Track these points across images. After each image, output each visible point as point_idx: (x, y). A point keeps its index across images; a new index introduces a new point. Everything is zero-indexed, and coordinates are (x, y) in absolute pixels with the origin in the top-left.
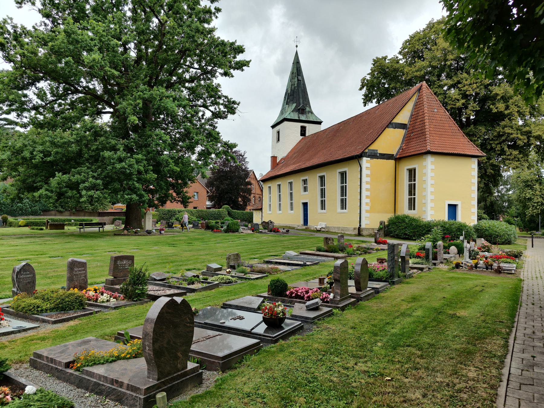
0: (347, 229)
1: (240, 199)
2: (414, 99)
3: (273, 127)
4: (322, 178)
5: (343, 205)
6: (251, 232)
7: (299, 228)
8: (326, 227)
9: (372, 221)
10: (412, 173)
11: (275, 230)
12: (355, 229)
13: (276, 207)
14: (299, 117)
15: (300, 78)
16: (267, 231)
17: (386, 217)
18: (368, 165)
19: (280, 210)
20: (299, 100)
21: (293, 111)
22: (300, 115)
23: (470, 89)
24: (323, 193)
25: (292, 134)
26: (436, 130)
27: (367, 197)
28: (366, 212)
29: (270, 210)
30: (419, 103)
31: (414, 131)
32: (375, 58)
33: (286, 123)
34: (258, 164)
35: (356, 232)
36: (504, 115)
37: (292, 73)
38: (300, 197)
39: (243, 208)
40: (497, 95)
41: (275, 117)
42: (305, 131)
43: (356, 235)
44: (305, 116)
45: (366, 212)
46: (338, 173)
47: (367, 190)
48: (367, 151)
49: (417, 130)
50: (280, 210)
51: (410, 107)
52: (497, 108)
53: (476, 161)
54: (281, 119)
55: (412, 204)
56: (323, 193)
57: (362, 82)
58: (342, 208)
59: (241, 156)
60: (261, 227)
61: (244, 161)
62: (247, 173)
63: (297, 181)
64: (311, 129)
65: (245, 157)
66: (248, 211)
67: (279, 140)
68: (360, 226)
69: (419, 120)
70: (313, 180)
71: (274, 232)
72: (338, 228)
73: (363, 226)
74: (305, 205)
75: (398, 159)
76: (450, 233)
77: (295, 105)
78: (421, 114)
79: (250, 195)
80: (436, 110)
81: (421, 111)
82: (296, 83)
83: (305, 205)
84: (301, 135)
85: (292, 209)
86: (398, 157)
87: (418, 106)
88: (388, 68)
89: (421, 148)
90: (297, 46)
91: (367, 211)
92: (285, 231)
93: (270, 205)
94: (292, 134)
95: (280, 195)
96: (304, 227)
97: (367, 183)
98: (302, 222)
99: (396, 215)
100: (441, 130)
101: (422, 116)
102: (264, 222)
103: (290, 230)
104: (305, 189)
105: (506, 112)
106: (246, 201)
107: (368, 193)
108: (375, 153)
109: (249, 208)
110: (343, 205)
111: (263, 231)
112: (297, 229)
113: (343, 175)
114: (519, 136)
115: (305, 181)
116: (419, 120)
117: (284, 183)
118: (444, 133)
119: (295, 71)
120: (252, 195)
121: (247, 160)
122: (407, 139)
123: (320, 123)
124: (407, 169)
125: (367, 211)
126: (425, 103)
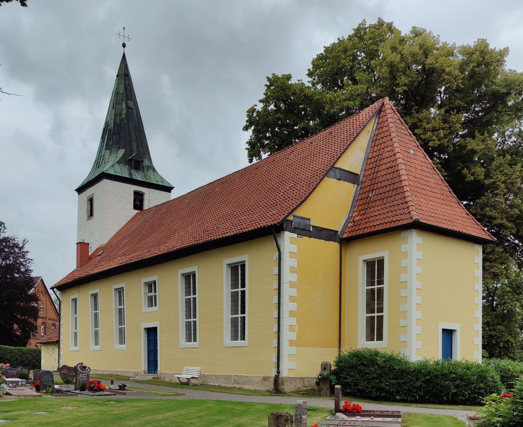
0: (248, 380)
1: (15, 326)
2: (371, 127)
3: (80, 190)
4: (190, 279)
5: (239, 330)
6: (33, 392)
7: (137, 378)
8: (202, 376)
9: (304, 362)
10: (375, 270)
11: (94, 387)
12: (265, 379)
13: (84, 338)
14: (130, 174)
15: (131, 104)
16: (72, 387)
17: (331, 357)
18: (294, 248)
19: (96, 343)
21: (118, 162)
22: (133, 171)
23: (434, 138)
24: (191, 308)
25: (117, 204)
26: (419, 185)
27: (292, 313)
28: (290, 345)
29: (76, 345)
30: (379, 137)
31: (376, 186)
32: (271, 77)
34: (50, 263)
35: (270, 386)
36: (483, 185)
37: (116, 93)
38: (141, 316)
39: (23, 341)
40: (473, 152)
41: (84, 174)
42: (142, 201)
43: (271, 393)
44: (141, 173)
45: (290, 345)
46: (180, 276)
47: (292, 299)
48: (291, 218)
49: (383, 184)
50: (96, 343)
51: (363, 142)
52: (473, 174)
53: (479, 249)
54: (97, 173)
55: (375, 329)
56: (191, 308)
57: (248, 116)
58: (189, 339)
59: (17, 247)
60: (57, 378)
61: (23, 257)
62: (30, 282)
63: (134, 286)
64: (153, 198)
65: (25, 250)
66: (33, 347)
67: (91, 214)
68: (278, 372)
69: (384, 167)
70: (169, 281)
71: (91, 389)
72: (227, 378)
73: (285, 373)
74: (152, 333)
75: (347, 241)
76: (466, 386)
77: (121, 152)
78: (387, 155)
79: (36, 321)
80: (412, 152)
81: (389, 149)
82: (124, 112)
83: (152, 333)
84: (136, 207)
85: (122, 341)
86: (345, 236)
87: (379, 141)
88: (294, 94)
89: (398, 218)
90: (124, 45)
91: (291, 343)
92: (115, 386)
93: (76, 334)
94: (117, 204)
95: (96, 315)
96: (150, 377)
97: (292, 285)
98: (143, 366)
99: (346, 350)
100: (425, 187)
101: (393, 158)
102: (65, 367)
103: (128, 385)
104: (152, 302)
105: (487, 182)
106: (29, 330)
107: (294, 306)
108: (305, 225)
109: (32, 344)
110: (239, 330)
111: (64, 388)
112: (137, 381)
113: (238, 272)
114: (505, 221)
115: (151, 286)
116: (384, 167)
117: (106, 291)
118: (430, 194)
119: (122, 90)
120: (40, 321)
121: (28, 256)
122: (362, 203)
123: (168, 189)
124: (364, 261)
125: (291, 343)
126: (393, 135)
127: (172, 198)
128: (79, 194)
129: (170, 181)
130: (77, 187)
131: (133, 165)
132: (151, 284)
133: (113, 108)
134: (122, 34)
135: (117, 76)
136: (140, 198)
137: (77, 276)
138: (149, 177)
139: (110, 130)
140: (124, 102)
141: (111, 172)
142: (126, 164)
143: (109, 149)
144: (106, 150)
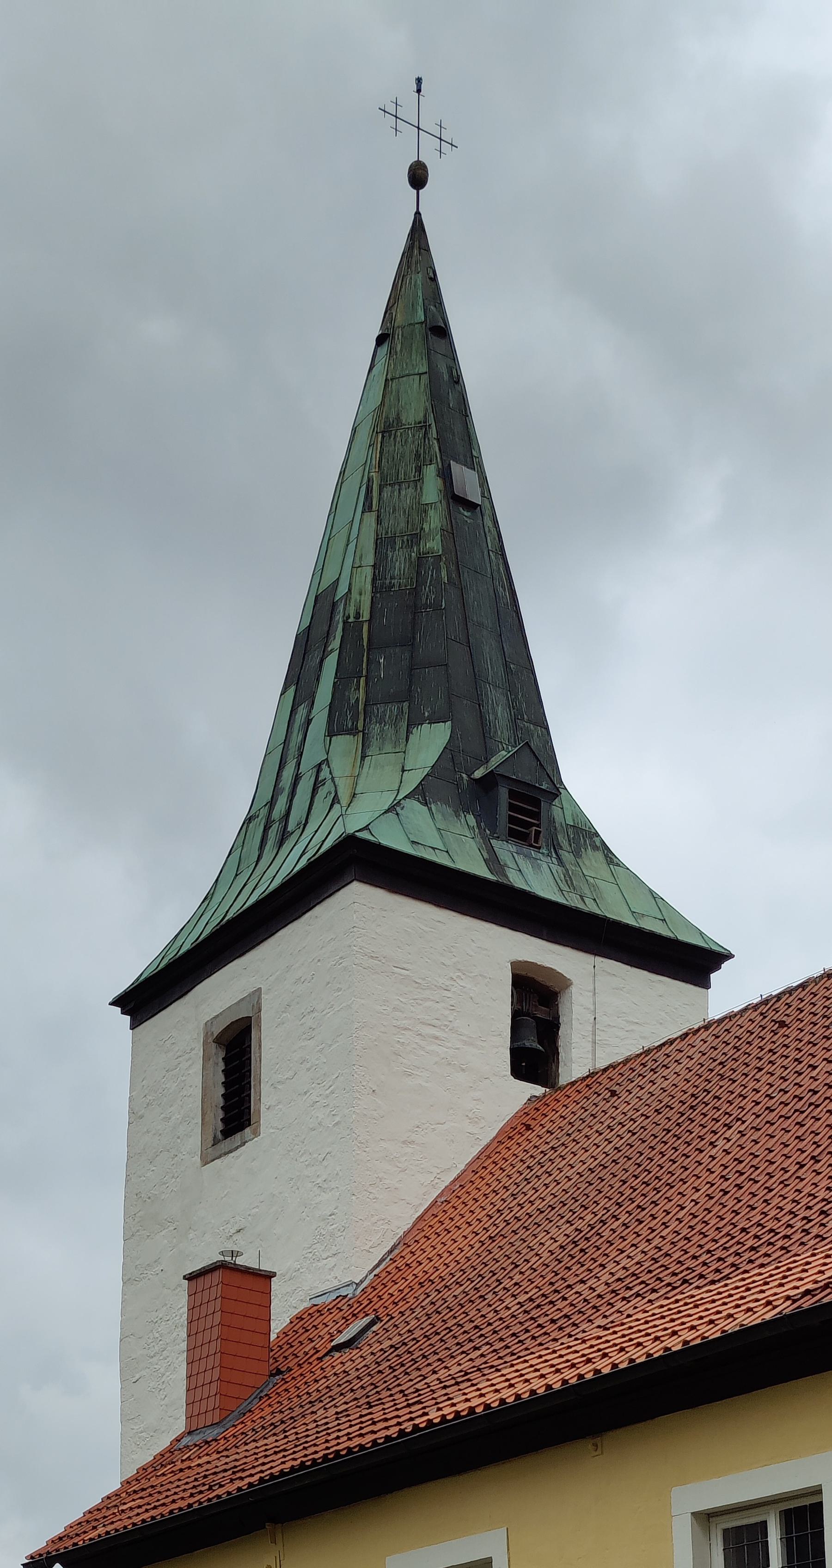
3: (142, 1001)
20: (479, 702)
21: (421, 793)
22: (505, 850)
33: (359, 903)
46: (683, 1531)
64: (614, 1014)
82: (435, 520)
90: (418, 177)
119: (414, 405)
123: (695, 963)
127: (716, 1011)
128: (133, 1027)
129: (702, 915)
130: (110, 1000)
131: (503, 811)
132: (763, 1527)
133: (368, 507)
134: (408, 112)
135: (381, 340)
136: (541, 1013)
137: (178, 1498)
138: (594, 888)
139: (351, 628)
140: (430, 471)
141: (391, 837)
142: (462, 806)
143: (352, 731)
144: (331, 733)
